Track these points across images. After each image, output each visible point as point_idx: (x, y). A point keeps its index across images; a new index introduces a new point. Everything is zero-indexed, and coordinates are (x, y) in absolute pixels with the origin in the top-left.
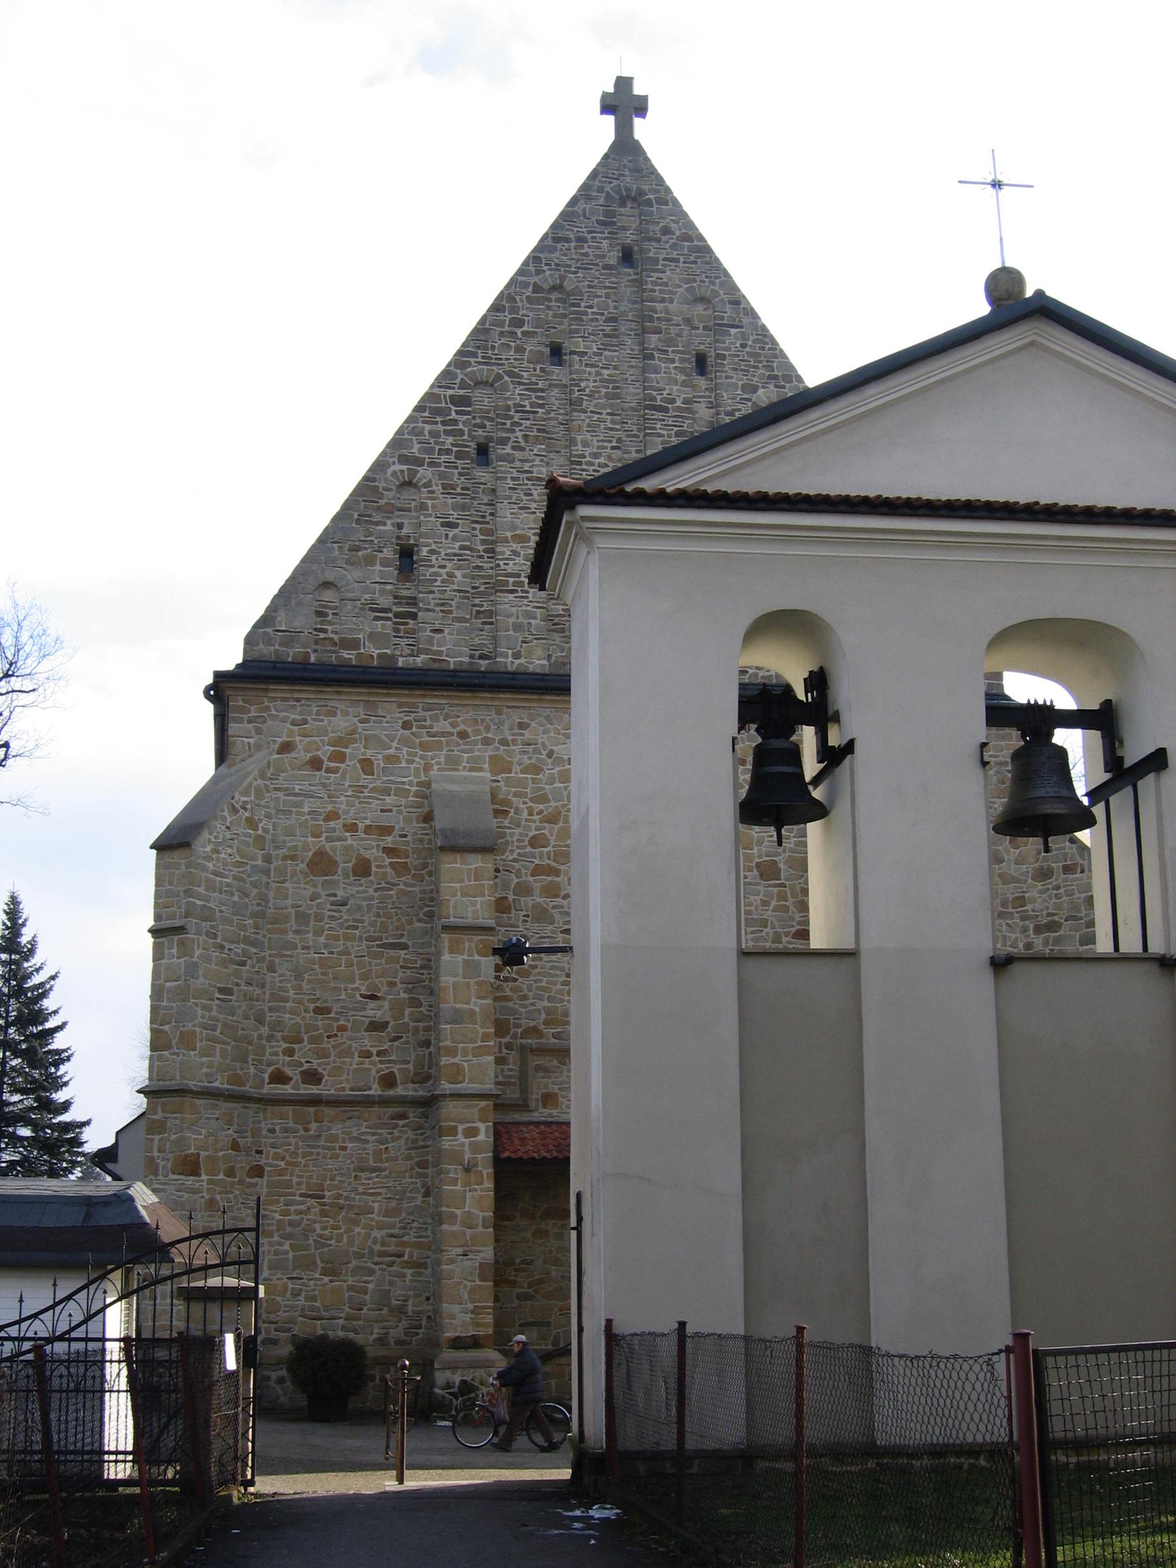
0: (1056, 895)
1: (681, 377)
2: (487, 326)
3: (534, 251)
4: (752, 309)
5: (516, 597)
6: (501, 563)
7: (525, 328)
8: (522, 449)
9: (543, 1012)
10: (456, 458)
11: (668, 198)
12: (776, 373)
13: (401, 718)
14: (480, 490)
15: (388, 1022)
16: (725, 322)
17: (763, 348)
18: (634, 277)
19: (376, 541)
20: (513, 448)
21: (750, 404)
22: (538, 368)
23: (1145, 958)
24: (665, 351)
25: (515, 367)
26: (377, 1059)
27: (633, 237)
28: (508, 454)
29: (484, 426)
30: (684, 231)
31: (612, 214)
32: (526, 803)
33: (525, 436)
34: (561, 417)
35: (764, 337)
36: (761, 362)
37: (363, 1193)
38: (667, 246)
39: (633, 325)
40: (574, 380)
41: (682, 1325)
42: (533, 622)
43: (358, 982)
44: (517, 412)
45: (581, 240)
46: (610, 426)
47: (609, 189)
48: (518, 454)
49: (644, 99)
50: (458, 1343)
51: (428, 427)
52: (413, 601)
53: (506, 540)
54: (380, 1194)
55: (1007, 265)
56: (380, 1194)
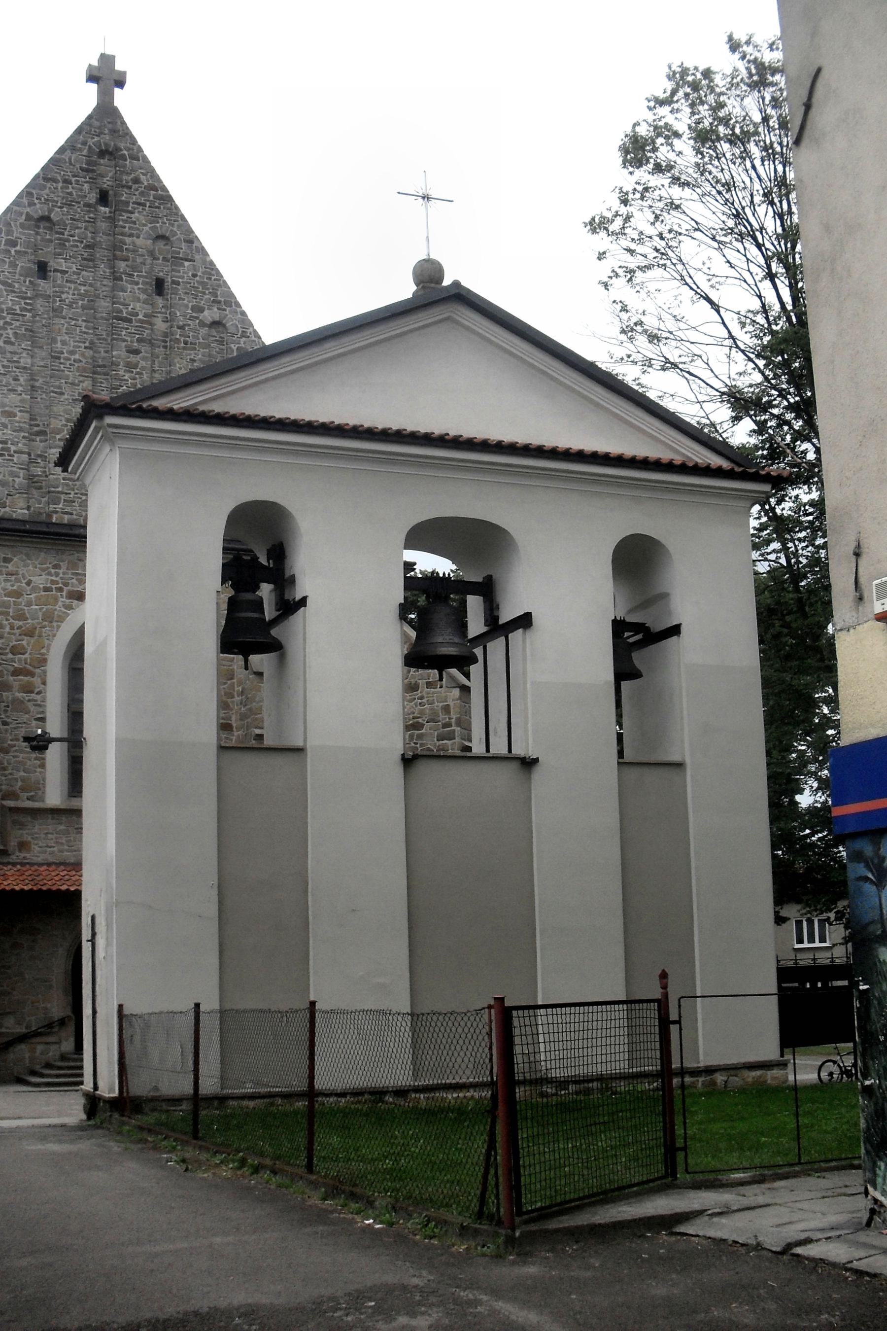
0: (420, 703)
1: (143, 297)
3: (27, 187)
4: (203, 247)
5: (4, 460)
7: (18, 248)
8: (13, 344)
9: (19, 780)
12: (219, 298)
16: (181, 256)
23: (509, 758)
24: (130, 275)
25: (9, 279)
27: (109, 183)
30: (150, 182)
31: (96, 164)
33: (15, 334)
34: (44, 321)
35: (211, 269)
36: (208, 289)
38: (137, 193)
39: (106, 253)
40: (56, 292)
41: (197, 1005)
42: (17, 479)
44: (8, 314)
45: (67, 182)
46: (84, 330)
48: (9, 348)
55: (432, 257)
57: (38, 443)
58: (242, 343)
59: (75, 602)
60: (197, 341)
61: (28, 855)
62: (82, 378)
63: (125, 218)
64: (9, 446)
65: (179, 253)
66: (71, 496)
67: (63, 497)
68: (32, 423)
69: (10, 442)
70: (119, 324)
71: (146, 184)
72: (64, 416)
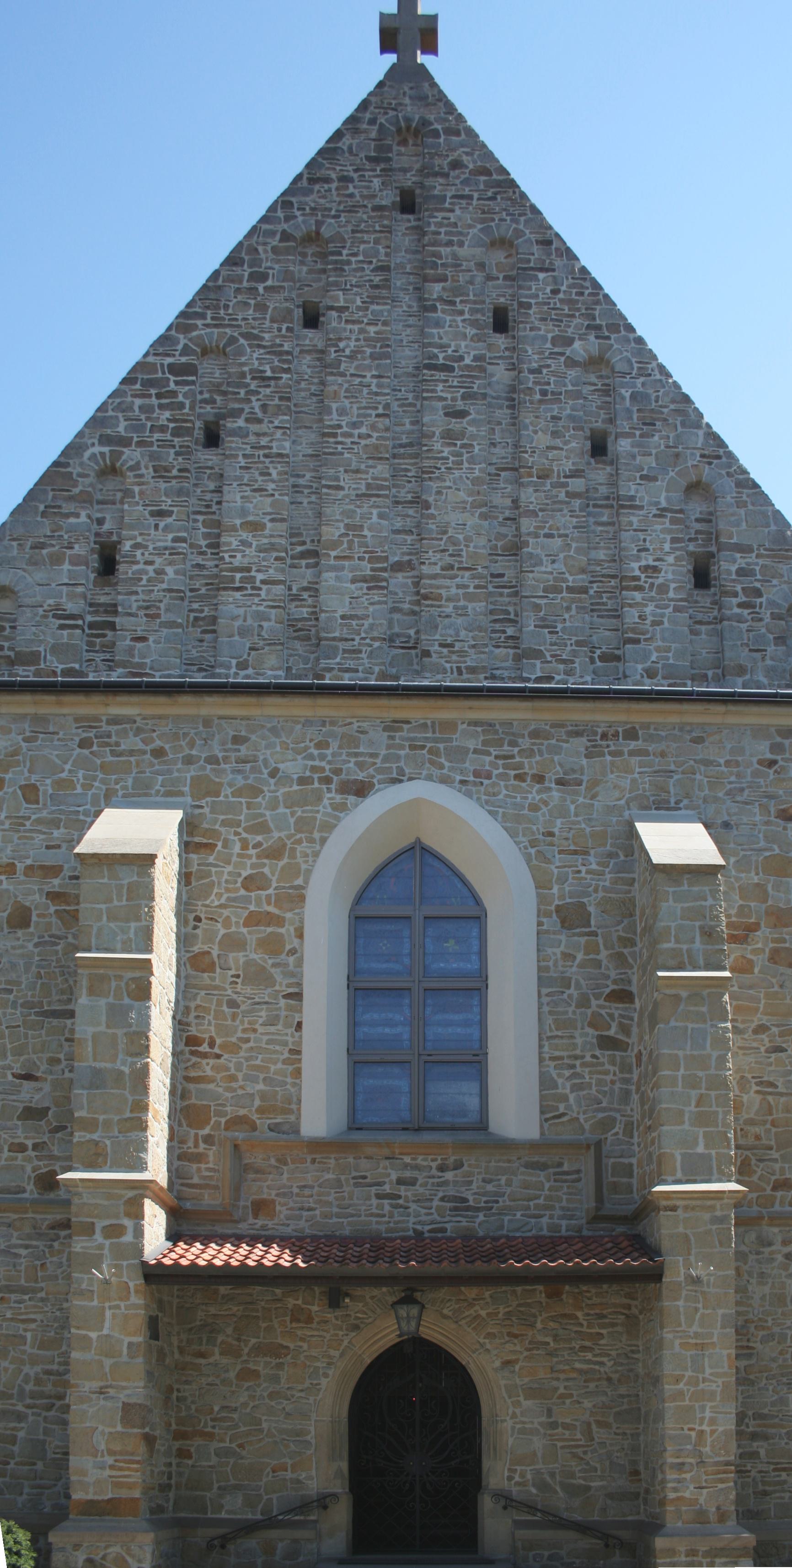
1: (471, 331)
2: (220, 282)
3: (283, 194)
6: (226, 556)
7: (269, 283)
8: (259, 421)
10: (173, 435)
11: (461, 127)
12: (598, 322)
13: (77, 735)
14: (206, 476)
15: (48, 1109)
16: (532, 265)
17: (582, 294)
18: (414, 223)
19: (66, 537)
20: (247, 420)
21: (562, 359)
22: (284, 327)
25: (253, 328)
26: (33, 1154)
27: (414, 179)
28: (240, 428)
29: (214, 402)
30: (479, 164)
32: (240, 834)
33: (264, 407)
34: (313, 388)
36: (578, 310)
37: (12, 1319)
38: (458, 182)
42: (265, 624)
43: (10, 1058)
44: (253, 378)
45: (345, 179)
47: (383, 121)
49: (433, 19)
50: (93, 1509)
51: (138, 402)
52: (112, 609)
53: (234, 529)
54: (34, 1321)
56: (34, 1321)
57: (303, 569)
58: (639, 385)
59: (352, 799)
60: (564, 389)
61: (270, 1224)
62: (371, 462)
63: (439, 220)
64: (253, 574)
65: (529, 261)
66: (355, 643)
67: (341, 645)
68: (294, 540)
69: (254, 569)
70: (432, 376)
71: (471, 166)
72: (342, 521)
